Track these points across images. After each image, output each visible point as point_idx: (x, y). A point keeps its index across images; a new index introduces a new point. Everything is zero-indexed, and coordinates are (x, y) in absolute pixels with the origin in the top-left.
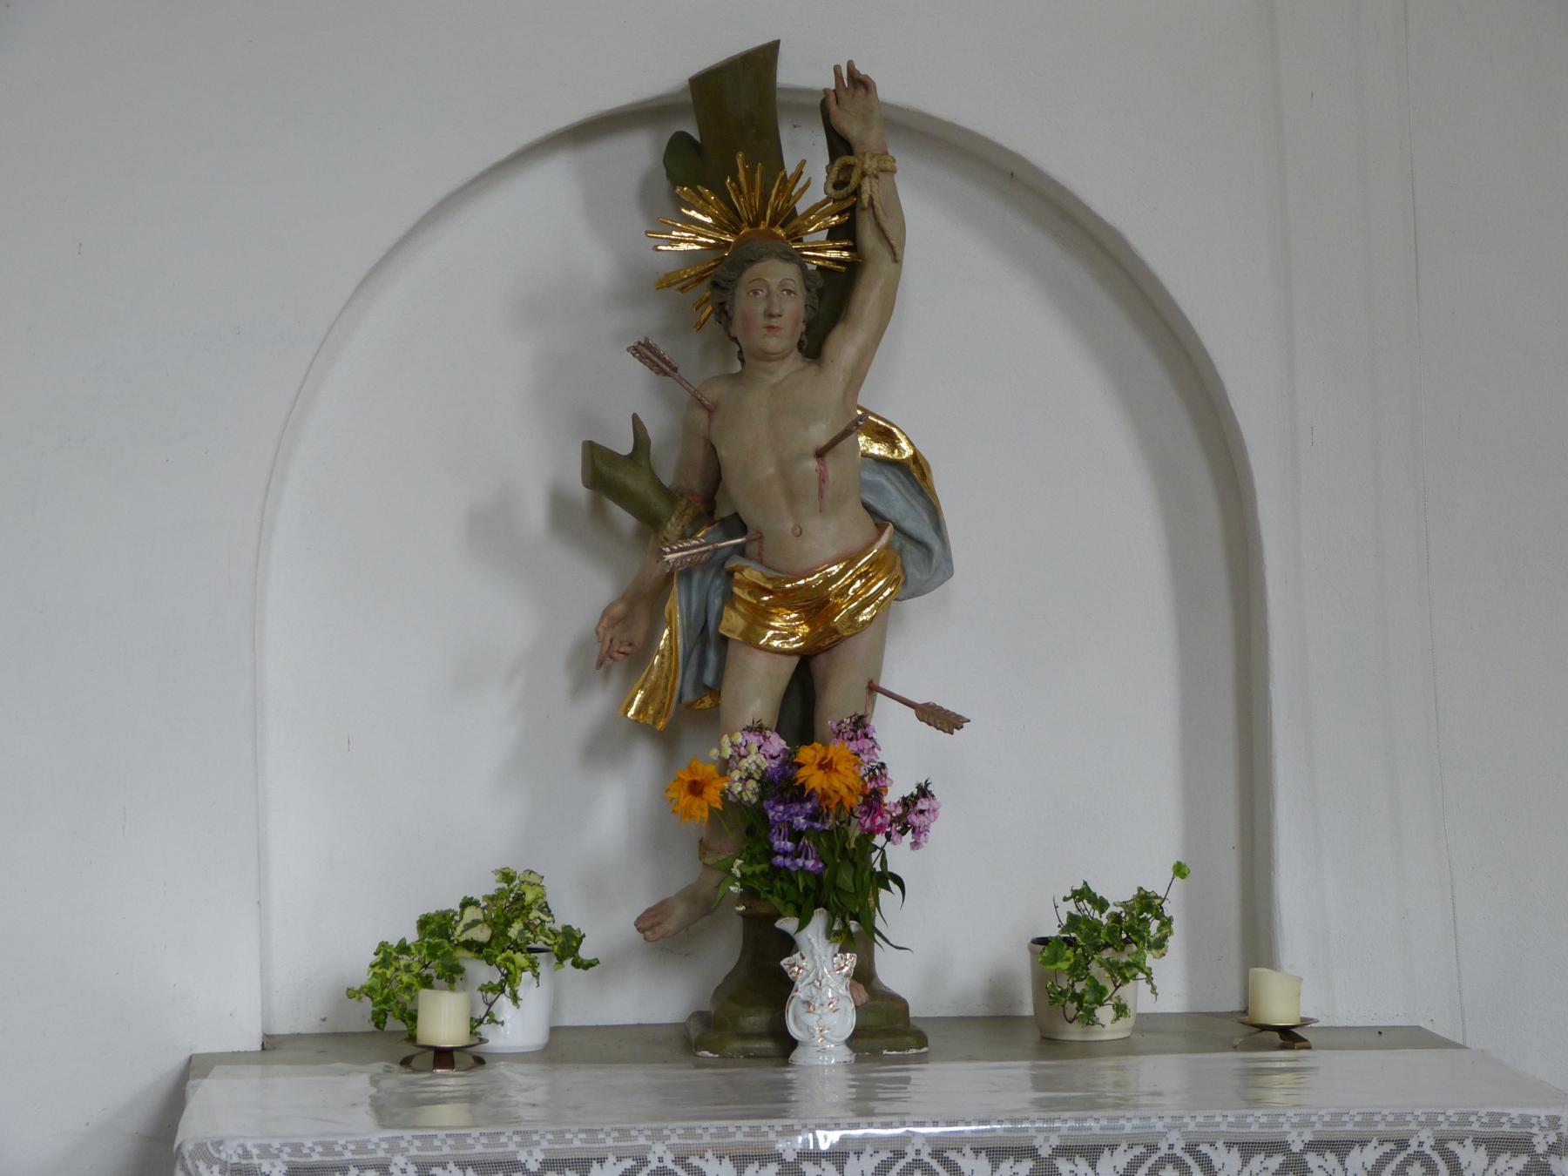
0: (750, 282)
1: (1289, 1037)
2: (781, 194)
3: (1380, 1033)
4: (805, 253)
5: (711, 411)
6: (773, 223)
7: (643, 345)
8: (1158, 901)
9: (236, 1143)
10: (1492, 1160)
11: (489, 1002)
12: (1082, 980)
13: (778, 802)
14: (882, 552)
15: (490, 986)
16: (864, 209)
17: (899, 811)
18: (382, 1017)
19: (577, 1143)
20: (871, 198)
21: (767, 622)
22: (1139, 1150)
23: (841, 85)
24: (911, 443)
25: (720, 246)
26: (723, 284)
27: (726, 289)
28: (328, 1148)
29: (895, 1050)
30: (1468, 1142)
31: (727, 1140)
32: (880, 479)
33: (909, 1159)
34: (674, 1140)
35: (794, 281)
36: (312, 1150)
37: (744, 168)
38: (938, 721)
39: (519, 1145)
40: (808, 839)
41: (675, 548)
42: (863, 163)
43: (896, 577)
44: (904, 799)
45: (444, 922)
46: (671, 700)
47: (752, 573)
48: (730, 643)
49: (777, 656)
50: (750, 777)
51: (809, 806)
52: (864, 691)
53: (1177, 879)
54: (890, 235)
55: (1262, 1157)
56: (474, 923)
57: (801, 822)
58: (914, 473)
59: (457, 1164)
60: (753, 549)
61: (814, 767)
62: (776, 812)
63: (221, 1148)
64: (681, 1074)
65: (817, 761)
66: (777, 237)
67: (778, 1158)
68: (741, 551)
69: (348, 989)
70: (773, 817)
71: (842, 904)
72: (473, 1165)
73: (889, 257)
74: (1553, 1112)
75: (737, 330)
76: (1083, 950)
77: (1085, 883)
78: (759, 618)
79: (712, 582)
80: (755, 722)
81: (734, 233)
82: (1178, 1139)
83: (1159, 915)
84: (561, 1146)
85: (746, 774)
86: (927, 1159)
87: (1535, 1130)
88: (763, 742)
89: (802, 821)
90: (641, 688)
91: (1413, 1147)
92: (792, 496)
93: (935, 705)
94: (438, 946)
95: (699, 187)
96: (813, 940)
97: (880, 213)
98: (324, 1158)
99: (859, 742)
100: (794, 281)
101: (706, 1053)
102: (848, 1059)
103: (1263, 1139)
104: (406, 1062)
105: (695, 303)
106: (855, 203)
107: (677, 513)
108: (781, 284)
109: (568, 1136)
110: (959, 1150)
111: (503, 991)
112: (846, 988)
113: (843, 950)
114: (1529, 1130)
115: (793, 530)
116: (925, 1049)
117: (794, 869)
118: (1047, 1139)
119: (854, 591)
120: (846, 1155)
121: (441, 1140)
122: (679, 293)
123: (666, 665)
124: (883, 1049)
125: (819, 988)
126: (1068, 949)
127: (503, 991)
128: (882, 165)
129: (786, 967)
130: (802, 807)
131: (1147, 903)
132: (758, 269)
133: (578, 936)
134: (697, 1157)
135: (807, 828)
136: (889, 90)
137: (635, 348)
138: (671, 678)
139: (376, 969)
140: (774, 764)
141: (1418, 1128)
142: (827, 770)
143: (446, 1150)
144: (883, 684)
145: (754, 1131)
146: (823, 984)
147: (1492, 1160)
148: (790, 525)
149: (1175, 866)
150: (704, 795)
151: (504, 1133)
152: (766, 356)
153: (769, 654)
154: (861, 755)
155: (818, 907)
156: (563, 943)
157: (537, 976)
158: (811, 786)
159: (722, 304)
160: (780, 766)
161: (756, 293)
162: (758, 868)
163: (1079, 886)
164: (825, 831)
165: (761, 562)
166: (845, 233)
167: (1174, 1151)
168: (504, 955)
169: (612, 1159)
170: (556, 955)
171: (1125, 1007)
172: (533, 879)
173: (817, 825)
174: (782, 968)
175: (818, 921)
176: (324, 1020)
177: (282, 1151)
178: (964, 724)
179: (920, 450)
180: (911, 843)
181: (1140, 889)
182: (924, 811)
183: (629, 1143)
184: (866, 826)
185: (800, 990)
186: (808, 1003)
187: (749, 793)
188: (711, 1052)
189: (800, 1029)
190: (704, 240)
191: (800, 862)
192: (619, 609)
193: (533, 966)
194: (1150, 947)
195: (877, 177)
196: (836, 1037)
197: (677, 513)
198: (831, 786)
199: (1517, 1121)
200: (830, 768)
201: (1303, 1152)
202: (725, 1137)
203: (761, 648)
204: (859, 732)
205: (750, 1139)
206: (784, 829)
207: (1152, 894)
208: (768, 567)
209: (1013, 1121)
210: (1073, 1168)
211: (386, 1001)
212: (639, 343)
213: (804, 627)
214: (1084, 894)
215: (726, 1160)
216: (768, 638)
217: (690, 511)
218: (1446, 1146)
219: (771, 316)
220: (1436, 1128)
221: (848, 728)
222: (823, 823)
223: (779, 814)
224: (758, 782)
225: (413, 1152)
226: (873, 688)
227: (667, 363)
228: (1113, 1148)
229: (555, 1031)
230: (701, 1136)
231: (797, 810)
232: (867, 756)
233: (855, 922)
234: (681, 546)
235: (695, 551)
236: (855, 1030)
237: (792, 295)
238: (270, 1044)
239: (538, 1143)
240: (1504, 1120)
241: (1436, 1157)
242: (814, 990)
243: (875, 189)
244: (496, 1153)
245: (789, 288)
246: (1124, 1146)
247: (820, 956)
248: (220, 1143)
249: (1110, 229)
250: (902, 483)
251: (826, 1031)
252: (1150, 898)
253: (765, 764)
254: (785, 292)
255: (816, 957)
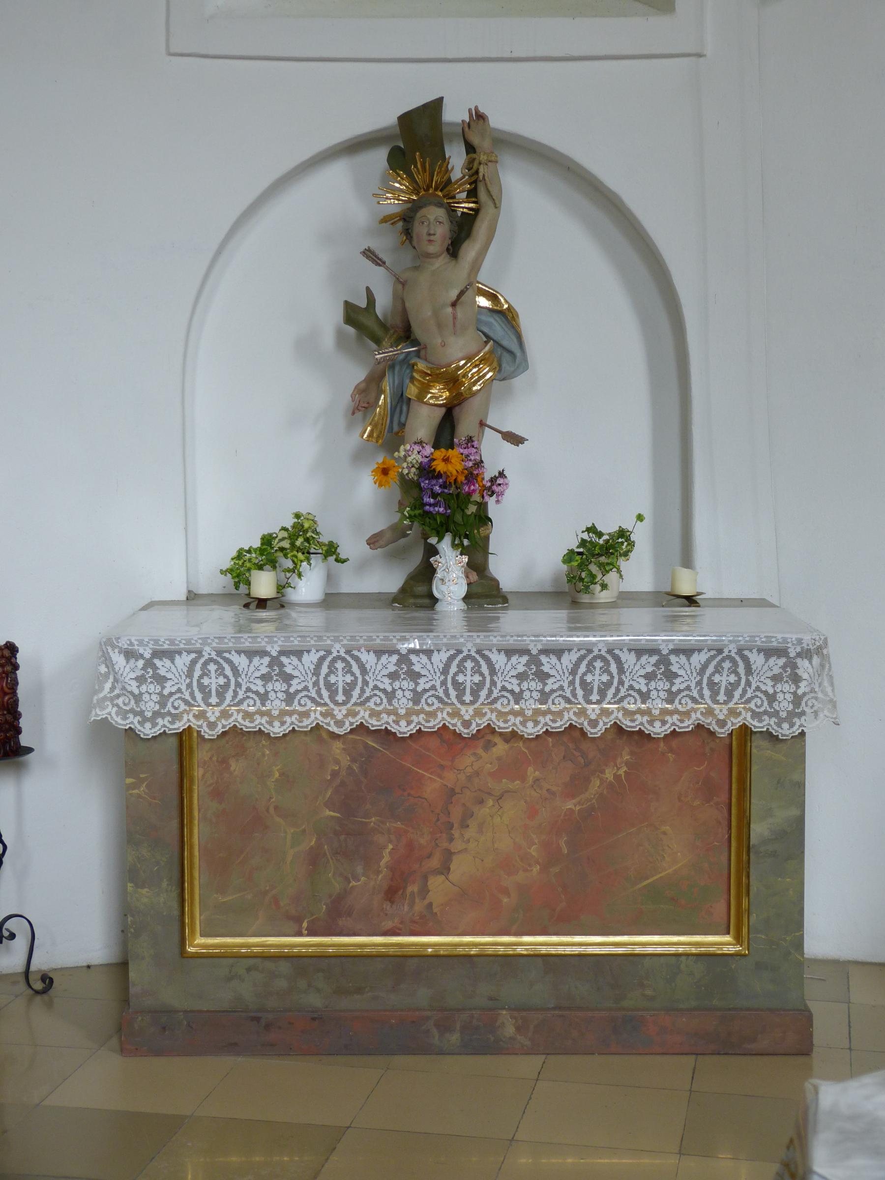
0: (420, 218)
1: (691, 600)
2: (439, 174)
3: (742, 601)
4: (452, 205)
5: (403, 284)
6: (436, 189)
7: (367, 250)
8: (628, 533)
9: (126, 639)
10: (767, 660)
11: (288, 577)
12: (585, 571)
13: (426, 479)
14: (487, 354)
15: (289, 569)
16: (481, 181)
17: (489, 484)
18: (238, 584)
19: (296, 643)
20: (484, 175)
21: (428, 390)
22: (583, 652)
23: (472, 118)
24: (506, 301)
25: (409, 201)
26: (407, 219)
27: (409, 222)
28: (172, 642)
29: (491, 605)
30: (754, 651)
31: (372, 643)
32: (491, 320)
33: (464, 654)
34: (345, 642)
35: (443, 217)
36: (164, 642)
37: (420, 161)
38: (511, 440)
39: (267, 643)
40: (441, 498)
41: (381, 352)
42: (480, 157)
43: (494, 367)
44: (492, 478)
45: (270, 538)
46: (384, 430)
47: (421, 365)
48: (411, 401)
49: (433, 407)
50: (413, 466)
51: (441, 481)
52: (478, 425)
53: (639, 522)
54: (493, 193)
55: (647, 657)
56: (283, 539)
57: (437, 489)
58: (508, 317)
59: (236, 651)
60: (423, 353)
61: (440, 460)
62: (425, 484)
63: (119, 640)
64: (388, 614)
65: (442, 457)
66: (439, 196)
67: (397, 652)
68: (418, 354)
69: (221, 570)
70: (423, 486)
71: (457, 530)
72: (244, 652)
73: (493, 206)
74: (799, 636)
75: (415, 243)
76: (586, 556)
77: (593, 524)
78: (425, 389)
79: (405, 370)
80: (419, 439)
81: (417, 194)
82: (603, 647)
83: (628, 539)
84: (289, 644)
85: (411, 465)
86: (474, 654)
87: (789, 645)
88: (421, 449)
89: (438, 488)
90: (370, 424)
91: (726, 653)
92: (440, 326)
93: (512, 432)
94: (265, 550)
95: (397, 171)
96: (445, 549)
97: (488, 183)
98: (170, 647)
99: (469, 449)
100: (443, 217)
101: (397, 604)
102: (462, 608)
103: (647, 647)
104: (247, 606)
105: (400, 232)
106: (477, 178)
107: (388, 336)
108: (435, 219)
109: (292, 639)
110: (490, 650)
111: (294, 572)
112: (462, 573)
113: (461, 554)
114: (786, 645)
115: (441, 343)
116: (506, 605)
117: (434, 513)
118: (535, 645)
119: (472, 374)
120: (432, 651)
121: (228, 639)
122: (391, 225)
123: (382, 413)
124: (484, 604)
125: (448, 573)
126: (577, 556)
127: (294, 572)
128: (490, 159)
129: (432, 562)
130: (437, 481)
131: (622, 533)
132: (424, 211)
133: (336, 546)
134: (357, 651)
135: (441, 492)
136: (498, 121)
137: (364, 252)
138: (385, 419)
139: (235, 560)
140: (426, 460)
141: (729, 643)
142: (447, 462)
143: (231, 645)
144: (488, 423)
145: (386, 638)
146: (450, 570)
147: (767, 660)
148: (439, 341)
149: (637, 516)
150: (389, 475)
151: (260, 637)
152: (428, 256)
153: (429, 406)
154: (470, 456)
155: (448, 532)
156: (328, 549)
157: (310, 565)
158: (438, 470)
159: (407, 230)
160: (429, 461)
161: (423, 223)
162: (417, 512)
163: (589, 526)
164: (450, 493)
165: (426, 360)
166: (473, 194)
167: (601, 653)
168: (292, 554)
169: (314, 651)
170: (324, 555)
171: (606, 585)
172: (310, 517)
173: (446, 491)
174: (430, 562)
175: (448, 539)
176: (224, 587)
177: (149, 643)
178: (525, 442)
179: (513, 305)
180: (496, 501)
181: (620, 527)
182: (501, 484)
183: (323, 643)
184: (466, 490)
185: (439, 573)
186: (442, 580)
187: (412, 474)
188: (398, 604)
189: (439, 593)
190: (404, 198)
191: (437, 509)
192: (363, 385)
193: (308, 560)
194: (621, 555)
195: (486, 164)
196: (455, 597)
197: (388, 336)
198: (448, 470)
199: (780, 640)
200: (448, 461)
201: (668, 654)
202: (371, 641)
203: (425, 403)
204: (469, 444)
205: (384, 642)
206: (429, 492)
207: (626, 530)
208: (429, 362)
209: (535, 636)
210: (549, 660)
211: (238, 576)
212: (366, 249)
213: (447, 392)
214: (592, 529)
215: (371, 653)
216: (429, 398)
217: (395, 336)
218: (743, 652)
219: (430, 235)
220: (738, 643)
221: (464, 442)
222: (449, 490)
223: (427, 485)
224: (417, 469)
225: (214, 645)
226: (482, 424)
227: (380, 260)
228: (570, 650)
229: (326, 594)
230: (358, 641)
231: (434, 482)
232: (474, 457)
233: (467, 540)
234: (384, 351)
235: (391, 354)
236: (466, 595)
237: (442, 224)
238: (192, 597)
239: (276, 642)
240: (773, 640)
241: (738, 658)
242: (445, 573)
243: (485, 171)
244: (256, 646)
245: (440, 221)
246: (575, 650)
247: (449, 557)
248: (119, 638)
249: (614, 194)
250: (503, 322)
251: (451, 594)
252: (624, 531)
253: (420, 459)
254: (438, 223)
255: (447, 557)
